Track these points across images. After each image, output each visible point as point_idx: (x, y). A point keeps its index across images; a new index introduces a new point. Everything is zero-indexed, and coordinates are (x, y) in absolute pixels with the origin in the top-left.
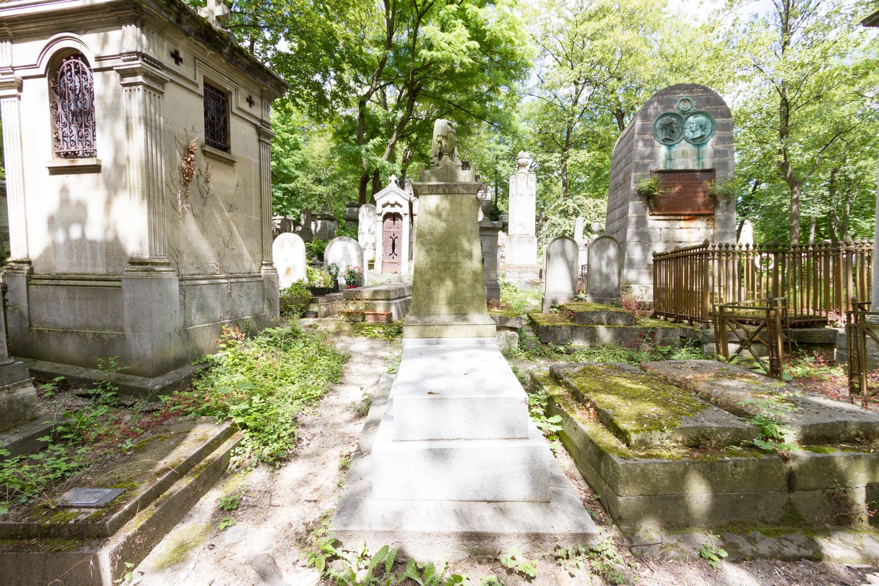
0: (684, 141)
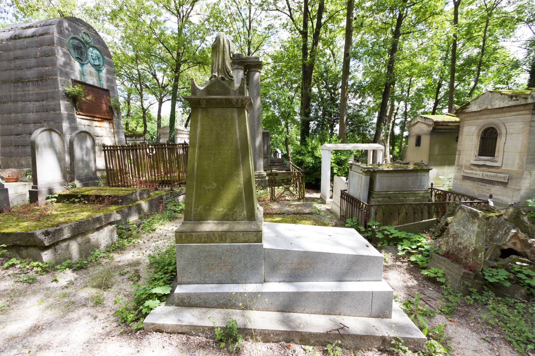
0: (89, 64)
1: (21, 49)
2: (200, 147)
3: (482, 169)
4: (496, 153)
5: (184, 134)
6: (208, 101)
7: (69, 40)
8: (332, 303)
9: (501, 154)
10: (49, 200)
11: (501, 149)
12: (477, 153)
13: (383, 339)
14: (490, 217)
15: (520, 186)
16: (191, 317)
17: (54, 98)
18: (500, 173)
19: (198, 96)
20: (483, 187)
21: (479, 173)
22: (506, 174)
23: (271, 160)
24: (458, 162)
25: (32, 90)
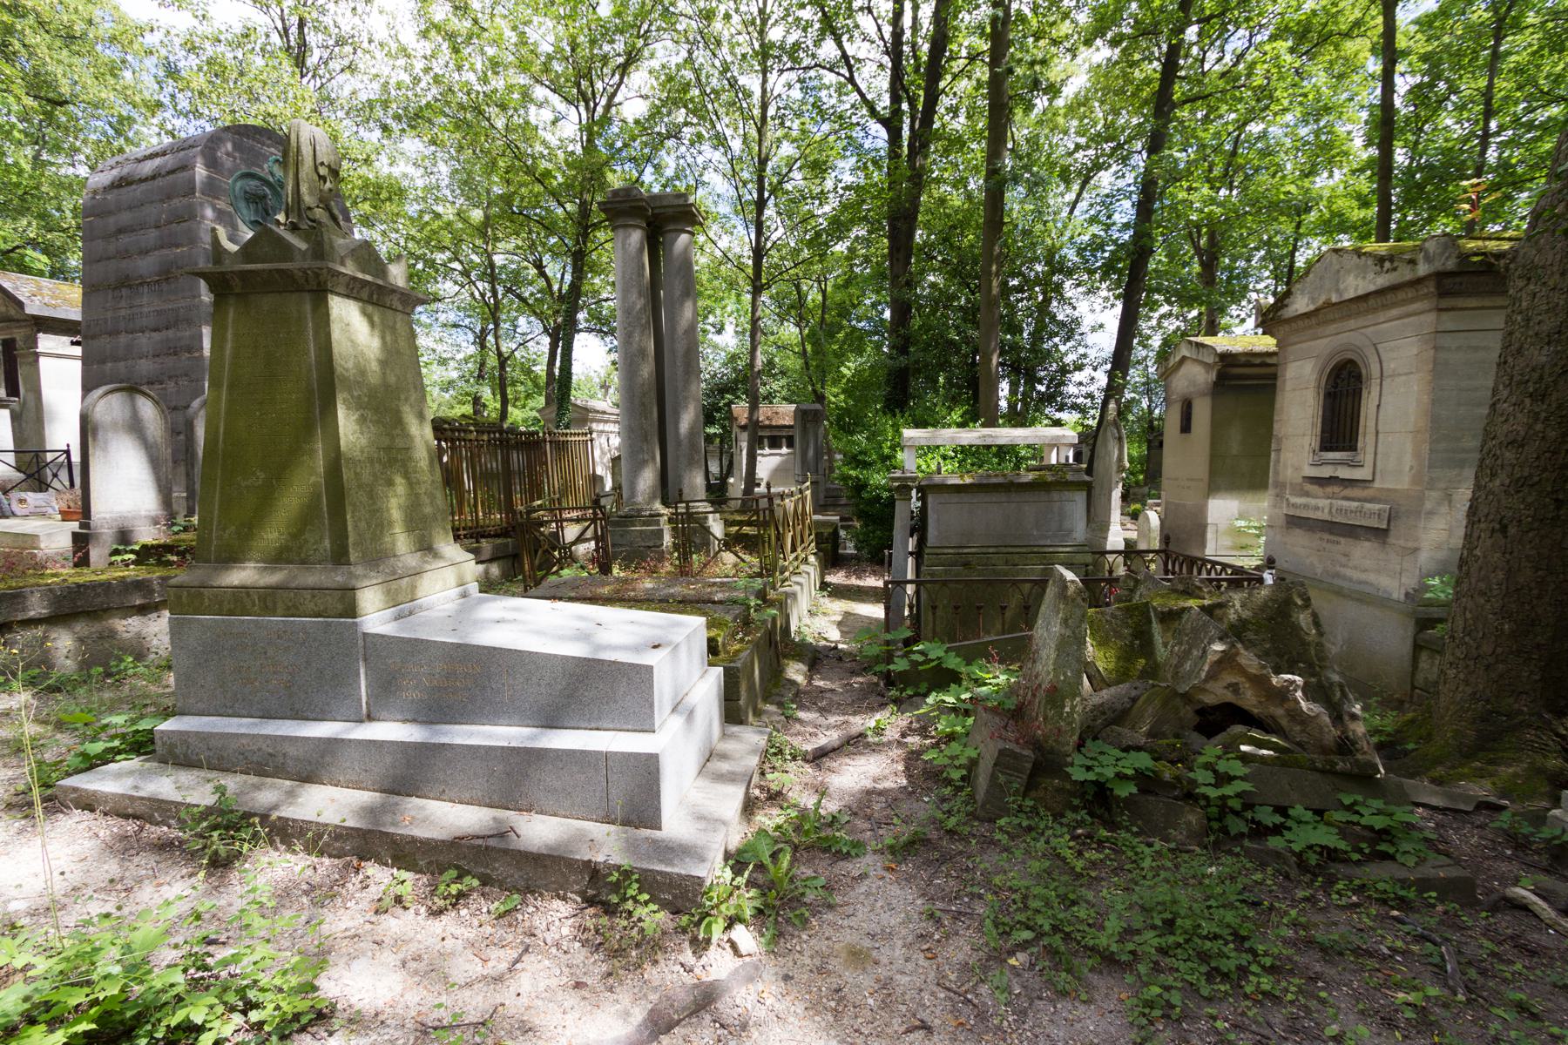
1: (130, 208)
2: (231, 387)
3: (1329, 490)
4: (1360, 438)
5: (606, 422)
6: (244, 276)
7: (235, 181)
8: (514, 778)
9: (1370, 439)
10: (119, 558)
11: (1371, 424)
12: (1316, 444)
13: (594, 873)
14: (1184, 610)
15: (1417, 539)
16: (166, 786)
17: (189, 322)
18: (1370, 501)
19: (228, 266)
20: (1329, 546)
21: (1321, 506)
22: (1386, 502)
23: (827, 490)
24: (1277, 473)
25: (148, 304)
